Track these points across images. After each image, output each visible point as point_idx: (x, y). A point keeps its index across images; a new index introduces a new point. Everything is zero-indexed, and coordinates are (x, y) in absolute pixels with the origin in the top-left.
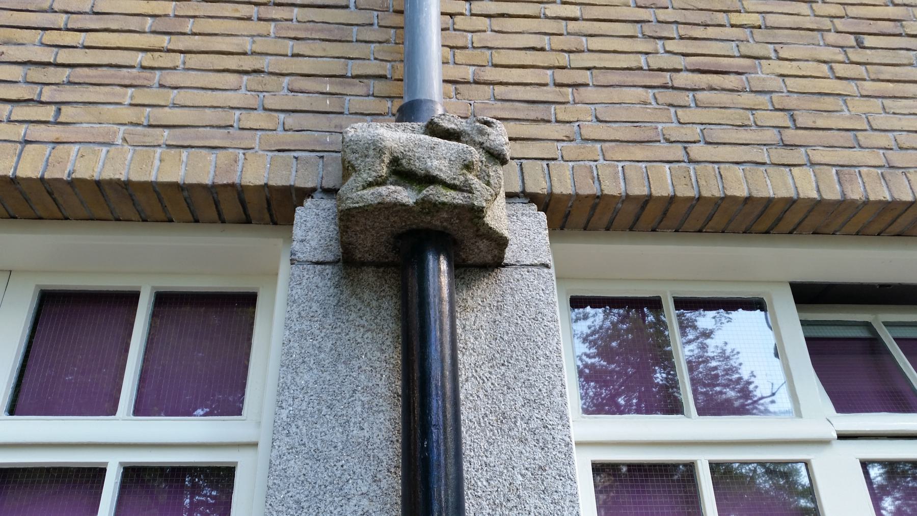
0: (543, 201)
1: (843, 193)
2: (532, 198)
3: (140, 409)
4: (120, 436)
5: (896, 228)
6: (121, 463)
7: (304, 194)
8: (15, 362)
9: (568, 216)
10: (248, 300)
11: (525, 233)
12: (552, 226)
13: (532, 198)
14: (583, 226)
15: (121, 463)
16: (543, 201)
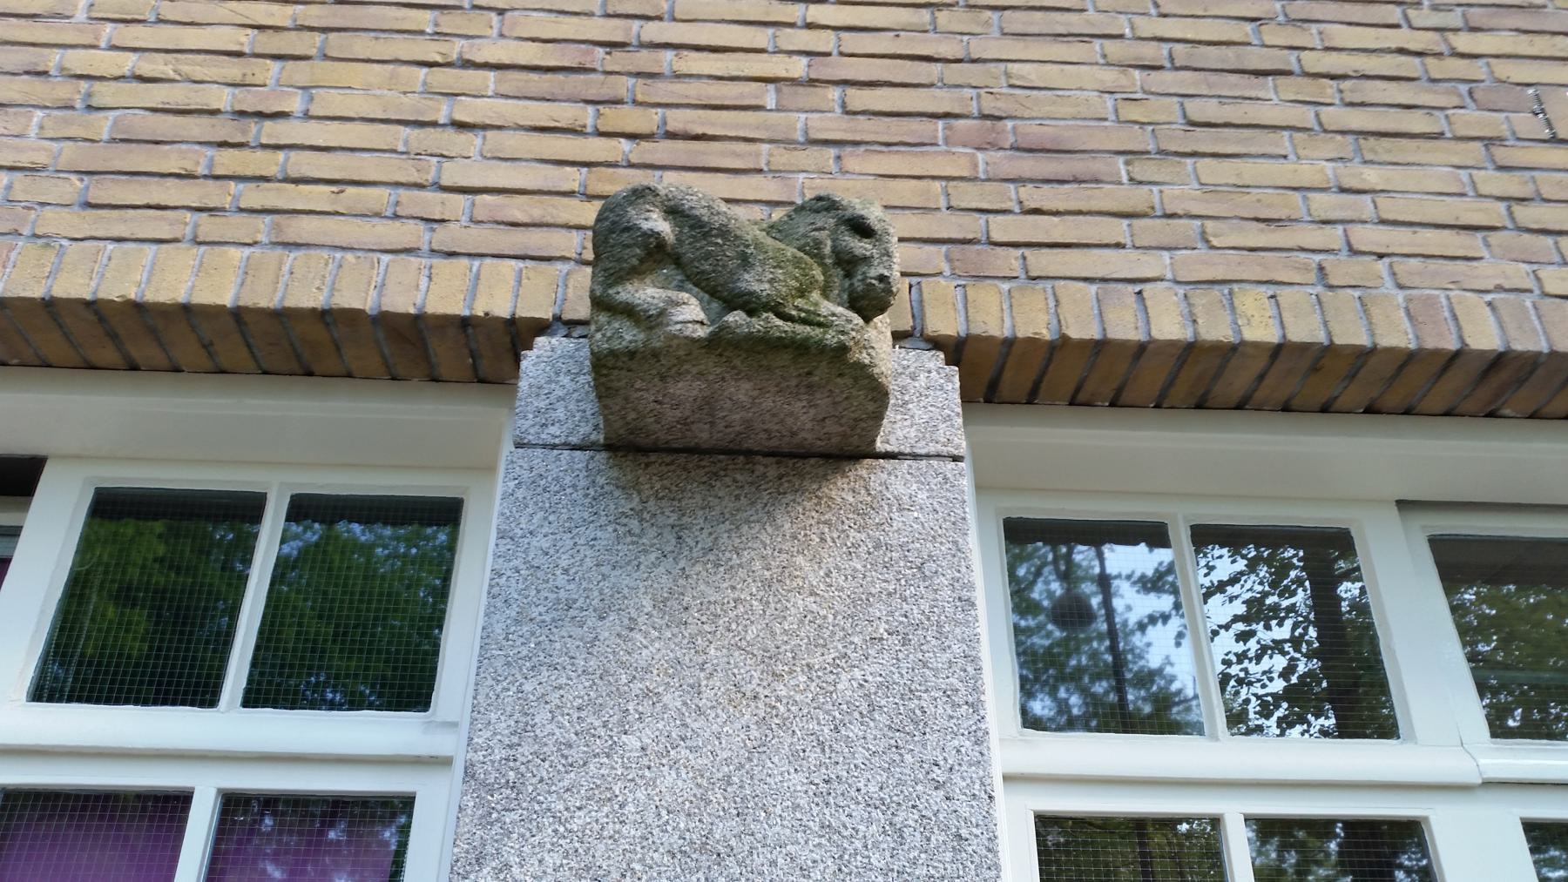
0: (955, 350)
1: (1196, 333)
2: (936, 343)
3: (254, 697)
4: (218, 745)
5: (1392, 400)
6: (219, 791)
7: (542, 327)
8: (42, 612)
9: (996, 377)
10: (447, 513)
11: (923, 400)
12: (967, 398)
13: (936, 343)
14: (1068, 396)
15: (219, 791)
16: (955, 350)
